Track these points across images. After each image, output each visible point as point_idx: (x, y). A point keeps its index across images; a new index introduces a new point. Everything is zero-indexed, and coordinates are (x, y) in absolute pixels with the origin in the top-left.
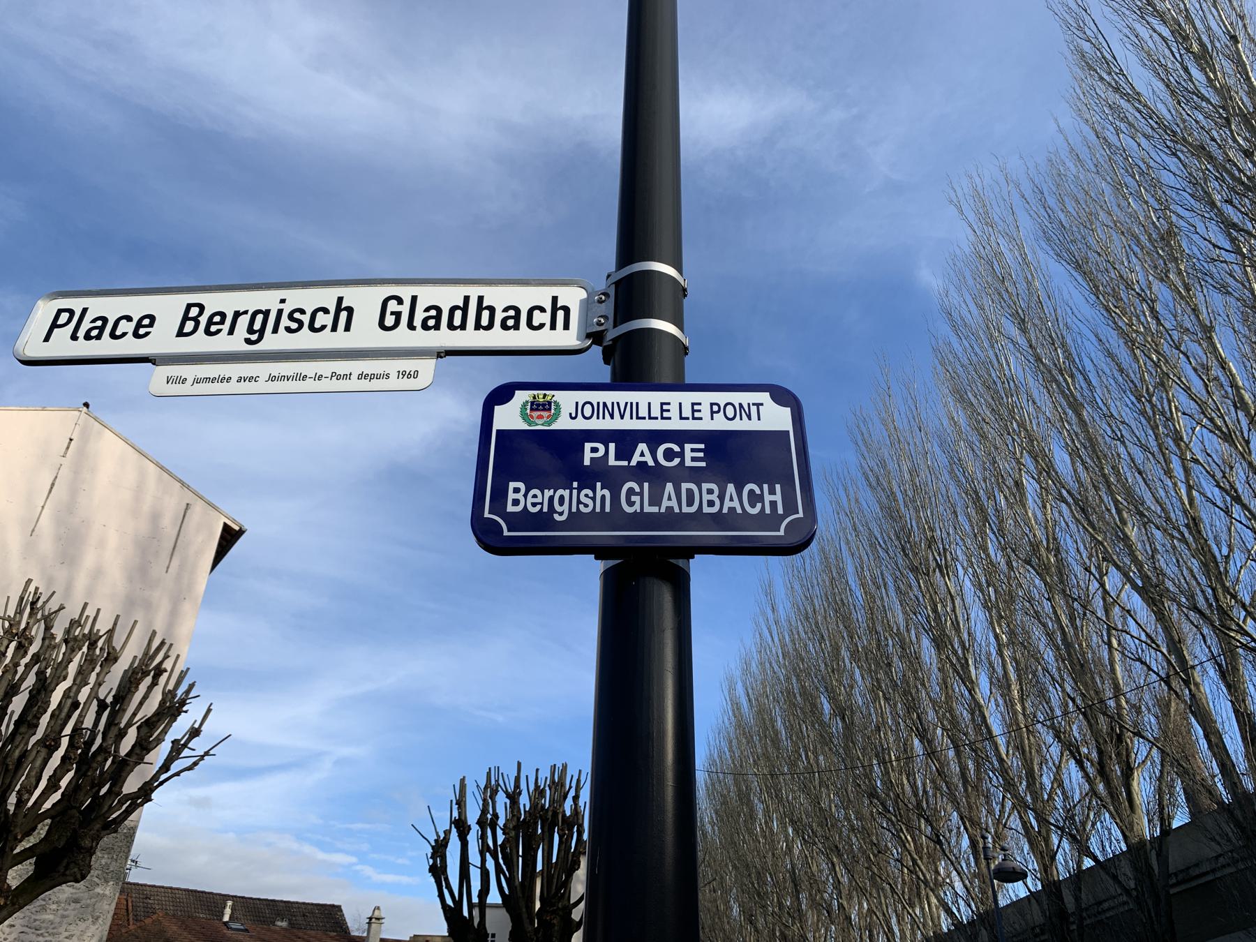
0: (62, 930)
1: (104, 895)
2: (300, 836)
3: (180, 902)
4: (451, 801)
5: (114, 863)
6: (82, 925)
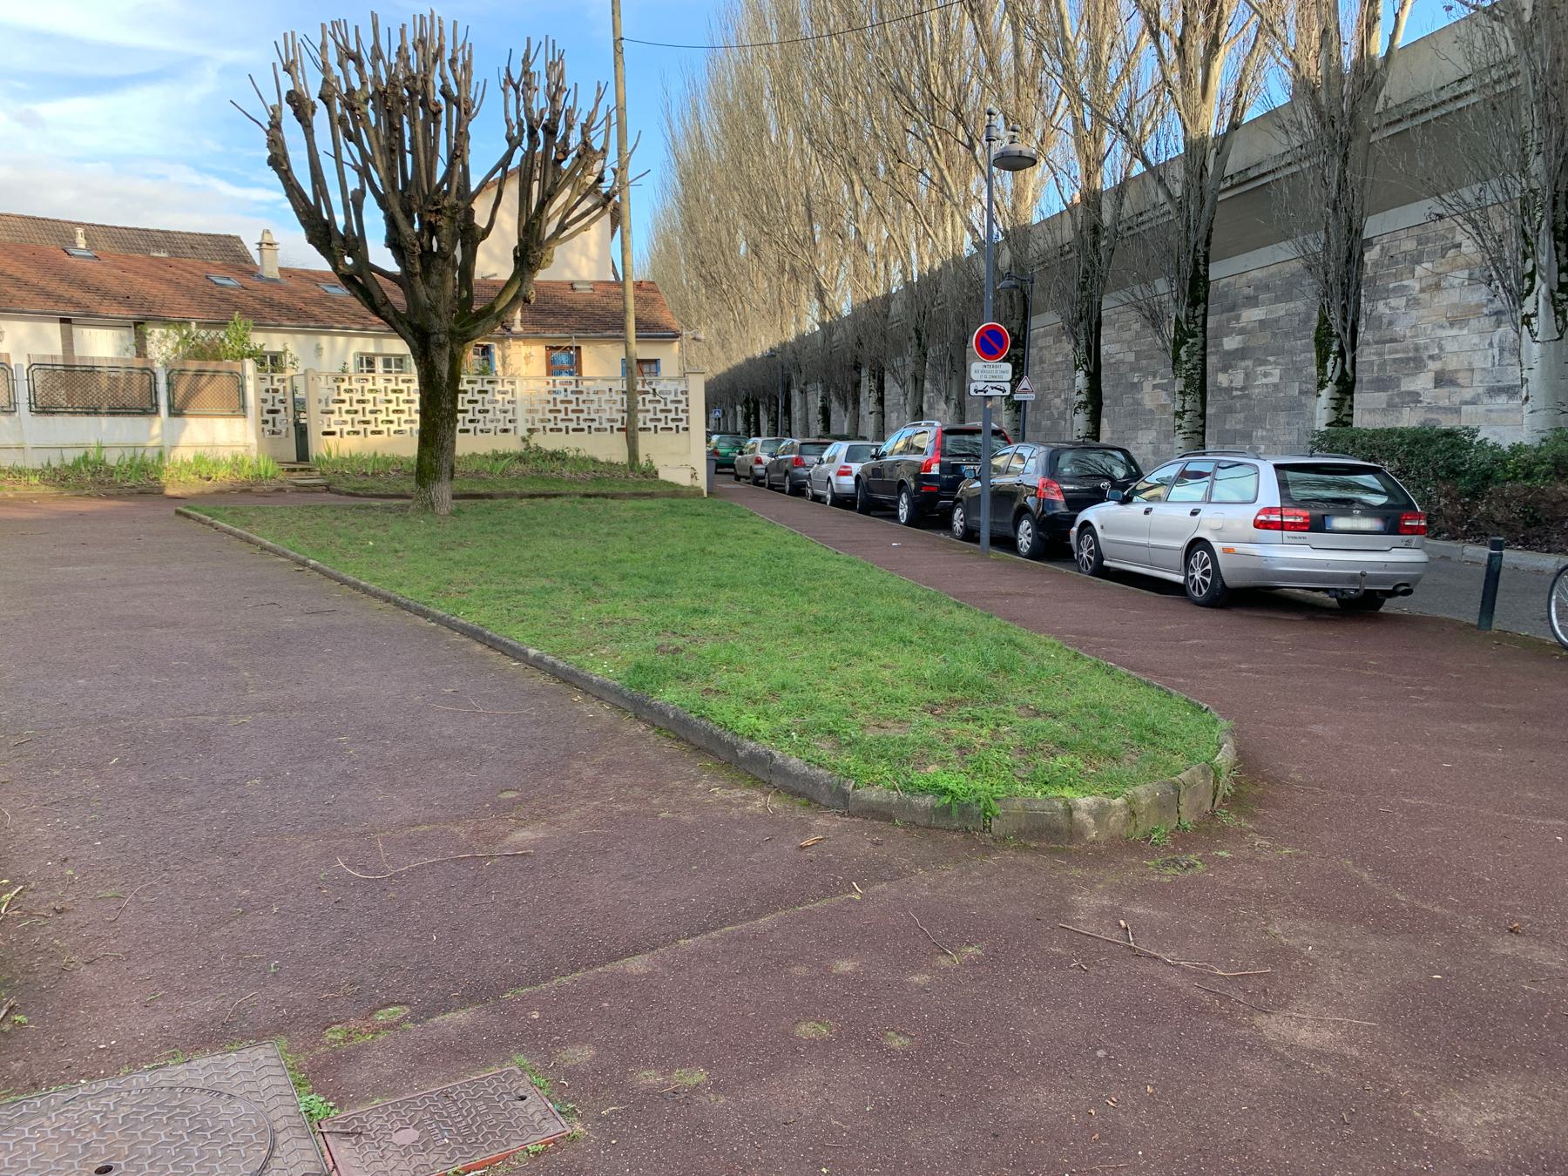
2: (198, 168)
3: (16, 231)
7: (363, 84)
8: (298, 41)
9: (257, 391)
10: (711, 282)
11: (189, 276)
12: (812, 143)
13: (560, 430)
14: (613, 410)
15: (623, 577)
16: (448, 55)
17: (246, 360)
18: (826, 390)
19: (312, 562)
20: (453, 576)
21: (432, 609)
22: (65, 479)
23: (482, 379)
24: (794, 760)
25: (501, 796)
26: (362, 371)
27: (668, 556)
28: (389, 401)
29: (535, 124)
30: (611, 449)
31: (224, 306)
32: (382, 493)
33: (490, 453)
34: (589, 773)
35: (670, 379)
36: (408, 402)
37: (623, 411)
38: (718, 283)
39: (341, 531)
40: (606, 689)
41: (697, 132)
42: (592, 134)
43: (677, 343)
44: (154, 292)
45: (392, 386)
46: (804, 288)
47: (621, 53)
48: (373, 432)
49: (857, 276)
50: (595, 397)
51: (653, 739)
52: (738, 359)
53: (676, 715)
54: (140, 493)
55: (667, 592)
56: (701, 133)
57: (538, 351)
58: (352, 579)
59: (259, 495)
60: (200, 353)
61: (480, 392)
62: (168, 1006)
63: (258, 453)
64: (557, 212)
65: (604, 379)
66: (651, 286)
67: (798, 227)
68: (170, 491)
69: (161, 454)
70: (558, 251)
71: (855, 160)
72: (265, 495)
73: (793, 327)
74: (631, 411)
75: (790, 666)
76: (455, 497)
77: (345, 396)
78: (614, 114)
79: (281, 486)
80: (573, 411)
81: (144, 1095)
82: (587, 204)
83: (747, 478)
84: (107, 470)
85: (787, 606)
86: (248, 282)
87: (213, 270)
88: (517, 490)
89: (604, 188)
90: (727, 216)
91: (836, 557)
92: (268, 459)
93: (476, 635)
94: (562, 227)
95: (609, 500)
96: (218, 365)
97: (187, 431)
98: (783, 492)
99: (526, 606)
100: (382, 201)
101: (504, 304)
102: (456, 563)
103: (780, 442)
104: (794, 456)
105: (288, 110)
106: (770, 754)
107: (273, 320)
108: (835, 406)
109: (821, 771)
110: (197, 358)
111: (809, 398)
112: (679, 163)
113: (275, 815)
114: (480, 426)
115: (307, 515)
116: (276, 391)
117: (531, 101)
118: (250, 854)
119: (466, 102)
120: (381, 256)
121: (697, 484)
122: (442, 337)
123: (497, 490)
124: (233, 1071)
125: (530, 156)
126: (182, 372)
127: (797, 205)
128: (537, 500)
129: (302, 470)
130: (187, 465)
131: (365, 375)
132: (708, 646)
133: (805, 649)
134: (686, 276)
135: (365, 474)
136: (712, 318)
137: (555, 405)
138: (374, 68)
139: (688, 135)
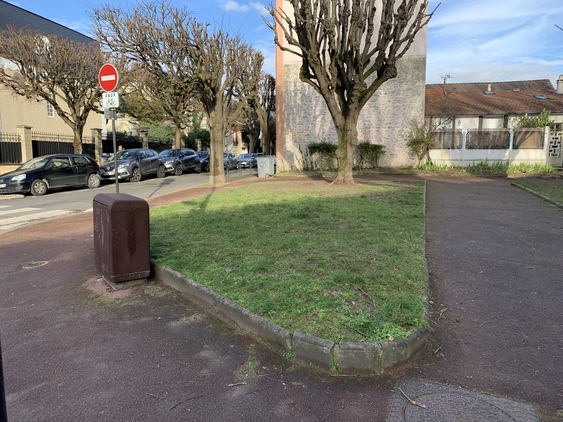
0: (407, 100)
1: (420, 86)
2: (535, 56)
6: (415, 98)
9: (548, 139)
22: (474, 171)
31: (539, 106)
44: (513, 104)
54: (498, 177)
59: (544, 179)
60: (528, 125)
68: (509, 176)
69: (508, 163)
72: (547, 179)
79: (554, 176)
81: (481, 403)
84: (488, 168)
86: (550, 96)
87: (536, 93)
92: (550, 165)
96: (534, 129)
97: (519, 154)
107: (559, 110)
110: (526, 127)
113: (542, 309)
116: (557, 138)
124: (516, 410)
126: (520, 132)
130: (517, 167)
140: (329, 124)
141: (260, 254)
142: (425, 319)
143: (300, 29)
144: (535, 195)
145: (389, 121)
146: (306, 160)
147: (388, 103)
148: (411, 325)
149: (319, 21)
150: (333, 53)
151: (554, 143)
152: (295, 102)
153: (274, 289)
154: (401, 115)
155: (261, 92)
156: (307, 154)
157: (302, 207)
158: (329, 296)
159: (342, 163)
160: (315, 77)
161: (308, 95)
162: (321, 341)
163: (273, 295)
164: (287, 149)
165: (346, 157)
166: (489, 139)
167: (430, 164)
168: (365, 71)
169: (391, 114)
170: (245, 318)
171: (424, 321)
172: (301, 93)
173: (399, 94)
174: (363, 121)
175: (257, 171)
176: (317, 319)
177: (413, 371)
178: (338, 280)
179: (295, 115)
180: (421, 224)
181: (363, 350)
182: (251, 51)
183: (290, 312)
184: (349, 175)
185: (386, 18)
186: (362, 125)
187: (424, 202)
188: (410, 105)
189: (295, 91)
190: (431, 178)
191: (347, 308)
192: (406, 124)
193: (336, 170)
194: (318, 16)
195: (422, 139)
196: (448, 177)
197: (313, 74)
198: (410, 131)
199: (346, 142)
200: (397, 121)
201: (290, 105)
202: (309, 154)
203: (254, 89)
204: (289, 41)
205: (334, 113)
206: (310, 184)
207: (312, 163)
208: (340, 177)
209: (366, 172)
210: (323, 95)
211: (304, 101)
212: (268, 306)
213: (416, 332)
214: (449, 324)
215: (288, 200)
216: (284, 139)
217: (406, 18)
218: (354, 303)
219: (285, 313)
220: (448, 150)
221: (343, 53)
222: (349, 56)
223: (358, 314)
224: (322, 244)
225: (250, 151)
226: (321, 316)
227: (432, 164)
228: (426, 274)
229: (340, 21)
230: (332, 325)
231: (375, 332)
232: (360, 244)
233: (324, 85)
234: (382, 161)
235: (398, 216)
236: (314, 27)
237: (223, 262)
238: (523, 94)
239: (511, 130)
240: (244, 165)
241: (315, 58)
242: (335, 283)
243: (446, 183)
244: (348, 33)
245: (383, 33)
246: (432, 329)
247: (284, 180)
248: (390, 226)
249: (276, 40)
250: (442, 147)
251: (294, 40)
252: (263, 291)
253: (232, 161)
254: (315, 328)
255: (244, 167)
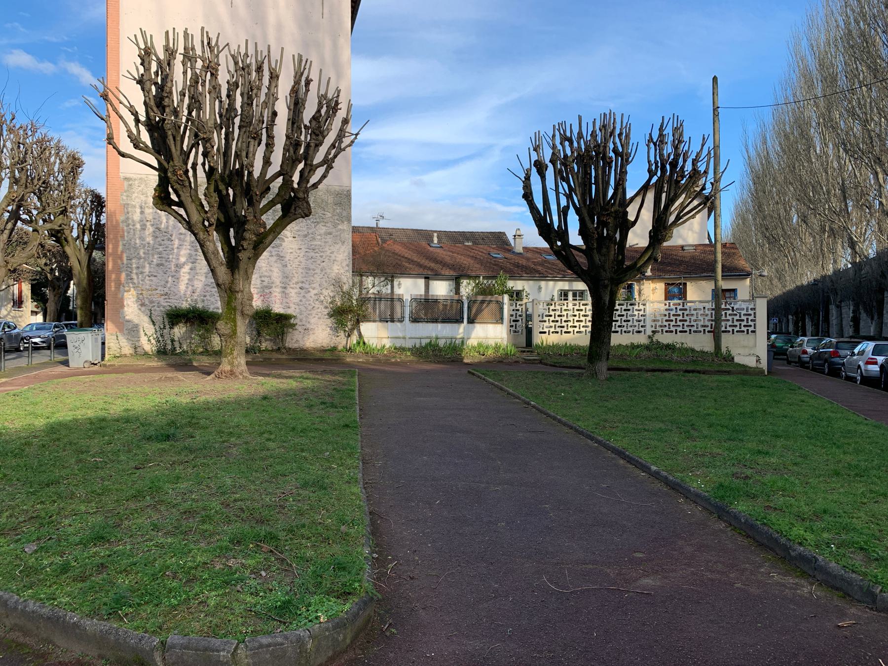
0: (327, 249)
1: (344, 230)
2: (488, 198)
4: (529, 148)
5: (344, 212)
6: (337, 246)
7: (572, 153)
8: (541, 135)
9: (509, 310)
10: (773, 241)
11: (481, 254)
12: (845, 150)
13: (672, 332)
14: (706, 321)
15: (710, 426)
16: (617, 132)
17: (505, 295)
18: (856, 306)
19: (532, 403)
20: (607, 417)
21: (595, 436)
22: (421, 353)
23: (627, 303)
24: (833, 564)
25: (634, 555)
26: (561, 300)
27: (741, 413)
28: (575, 316)
29: (665, 162)
30: (703, 343)
32: (569, 365)
33: (630, 345)
34: (688, 549)
35: (744, 301)
36: (585, 316)
37: (712, 321)
38: (777, 240)
39: (547, 386)
40: (699, 497)
41: (765, 153)
42: (699, 164)
43: (749, 279)
44: (465, 262)
45: (577, 307)
46: (840, 241)
47: (718, 115)
48: (566, 332)
49: (881, 232)
50: (694, 312)
51: (730, 534)
52: (790, 286)
53: (746, 520)
55: (741, 437)
56: (768, 153)
57: (660, 287)
58: (552, 414)
61: (625, 310)
62: (458, 641)
63: (508, 342)
64: (676, 209)
65: (700, 302)
66: (733, 245)
67: (835, 204)
68: (466, 361)
69: (463, 342)
70: (675, 231)
71: (879, 159)
72: (510, 364)
73: (831, 266)
74: (717, 320)
75: (830, 497)
76: (609, 369)
77: (552, 313)
78: (712, 152)
79: (517, 360)
80: (673, 315)
82: (695, 203)
83: (796, 362)
85: (827, 454)
86: (508, 255)
87: (492, 250)
88: (644, 367)
89: (706, 192)
90: (785, 200)
91: (866, 422)
93: (621, 454)
94: (678, 218)
95: (701, 375)
97: (475, 330)
98: (823, 373)
99: (650, 439)
100: (578, 211)
101: (643, 262)
102: (609, 409)
103: (821, 340)
104: (831, 350)
105: (534, 170)
106: (815, 557)
107: (519, 274)
108: (863, 316)
109: (854, 576)
111: (843, 311)
112: (752, 171)
114: (624, 329)
115: (531, 376)
116: (518, 310)
117: (663, 150)
118: (499, 565)
119: (626, 155)
120: (575, 239)
121: (760, 366)
122: (606, 282)
123: (632, 366)
125: (661, 180)
126: (475, 302)
127: (835, 190)
128: (656, 373)
129: (528, 351)
130: (473, 347)
131: (563, 302)
132: (768, 477)
133: (842, 486)
134: (755, 237)
135: (560, 355)
136: (773, 262)
137: (669, 317)
138: (579, 143)
139: (759, 155)
140: (203, 279)
141: (92, 511)
142: (368, 581)
143: (153, 127)
144: (497, 386)
145: (300, 279)
146: (161, 336)
147: (298, 251)
148: (349, 594)
149: (188, 120)
150: (210, 173)
151: (515, 316)
152: (142, 238)
153: (125, 570)
154: (318, 271)
155: (78, 216)
156: (164, 326)
157: (163, 420)
158: (224, 569)
159: (229, 344)
160: (180, 204)
161: (165, 230)
162: (216, 642)
163: (124, 582)
164: (127, 318)
165: (234, 332)
166: (438, 309)
167: (361, 344)
168: (264, 202)
169: (303, 269)
170: (73, 631)
171: (367, 584)
172: (152, 225)
173: (314, 239)
174: (261, 277)
175: (67, 355)
176: (206, 609)
177: (355, 663)
178: (237, 541)
179: (142, 260)
180: (355, 437)
181: (282, 644)
182: (58, 149)
183: (157, 605)
184: (239, 363)
185: (292, 130)
186: (259, 282)
187: (357, 402)
188: (330, 257)
189: (141, 221)
190: (364, 365)
191: (253, 583)
192: (325, 284)
193: (218, 353)
194: (186, 112)
195: (349, 307)
196: (387, 362)
197: (176, 199)
198: (332, 294)
199: (235, 309)
200: (312, 279)
201: (133, 243)
202: (168, 327)
203: (64, 212)
204: (134, 145)
205: (214, 263)
206: (172, 379)
207: (173, 341)
208: (225, 366)
209: (267, 356)
210: (195, 235)
211: (159, 239)
212: (117, 601)
213: (356, 604)
214: (400, 585)
215: (134, 410)
216: (122, 299)
217: (322, 133)
218: (263, 573)
219: (149, 608)
220: (386, 324)
221: (227, 172)
222: (236, 178)
223: (271, 590)
224: (205, 483)
225: (48, 318)
226: (212, 603)
227: (364, 343)
228: (366, 515)
229: (221, 123)
230: (232, 614)
231: (299, 612)
232: (267, 477)
233: (196, 217)
234: (292, 340)
235: (321, 428)
236: (180, 128)
237: (17, 535)
238: (476, 250)
239: (464, 298)
240: (35, 343)
241: (181, 176)
242: (231, 546)
243: (384, 372)
244: (234, 143)
245: (288, 150)
246: (378, 594)
247: (123, 372)
248: (311, 443)
249: (110, 140)
250: (378, 319)
251: (144, 143)
252: (105, 576)
253: (10, 337)
254: (204, 625)
255: (36, 348)
